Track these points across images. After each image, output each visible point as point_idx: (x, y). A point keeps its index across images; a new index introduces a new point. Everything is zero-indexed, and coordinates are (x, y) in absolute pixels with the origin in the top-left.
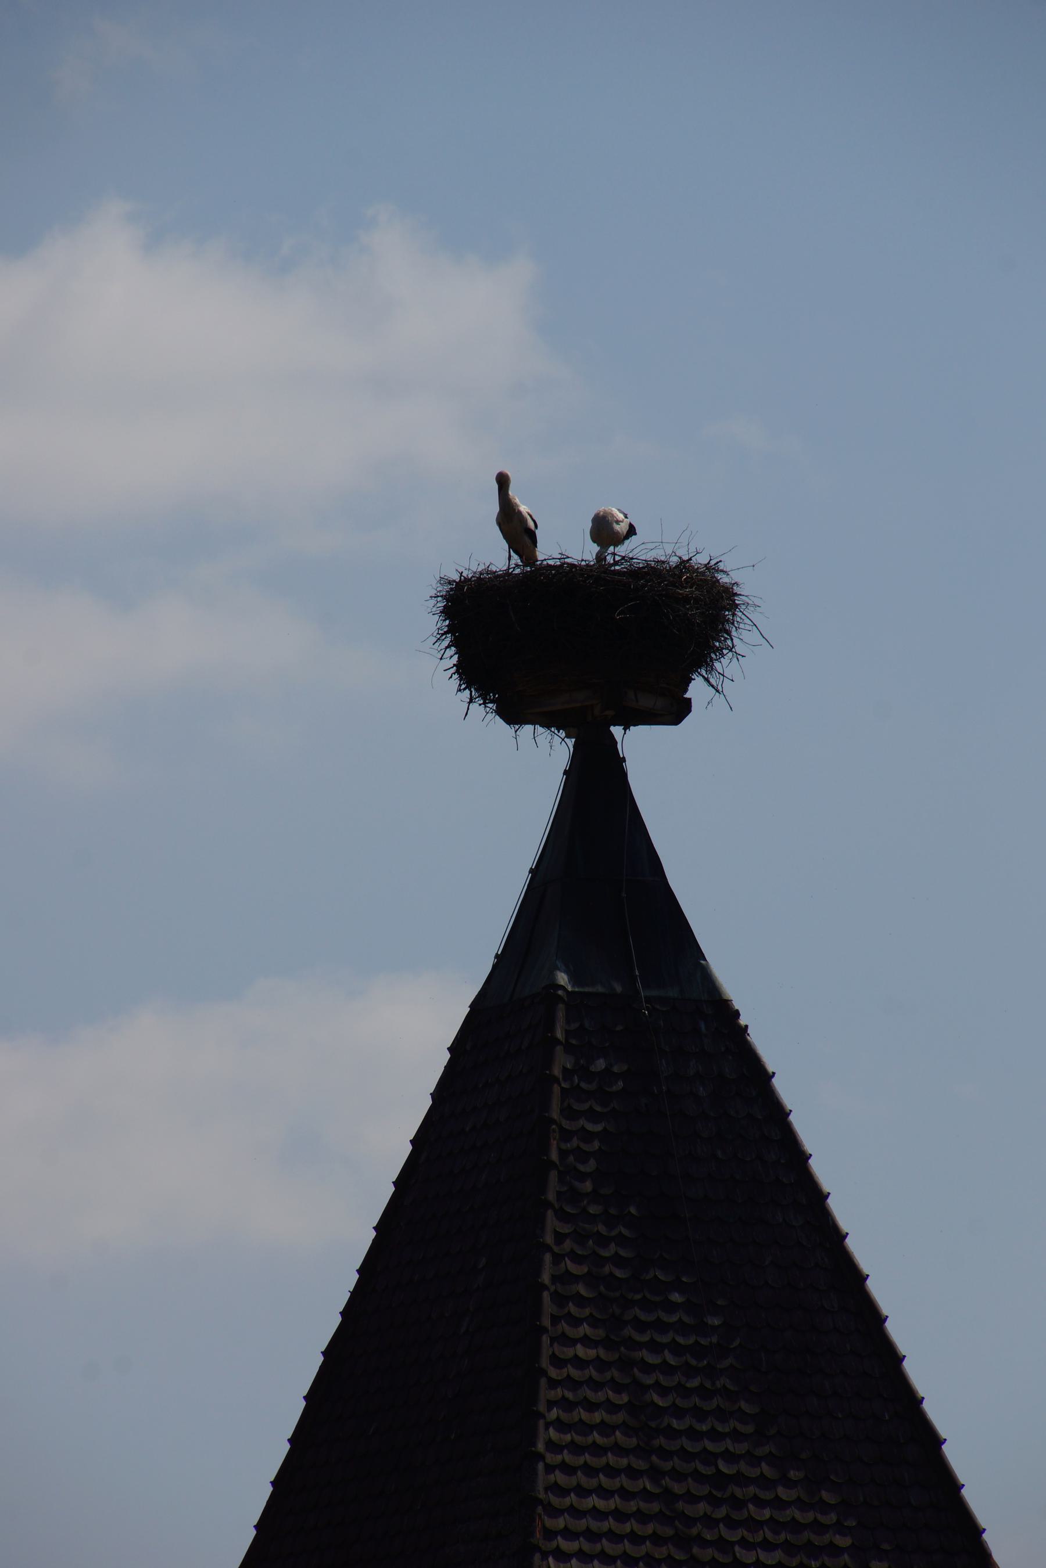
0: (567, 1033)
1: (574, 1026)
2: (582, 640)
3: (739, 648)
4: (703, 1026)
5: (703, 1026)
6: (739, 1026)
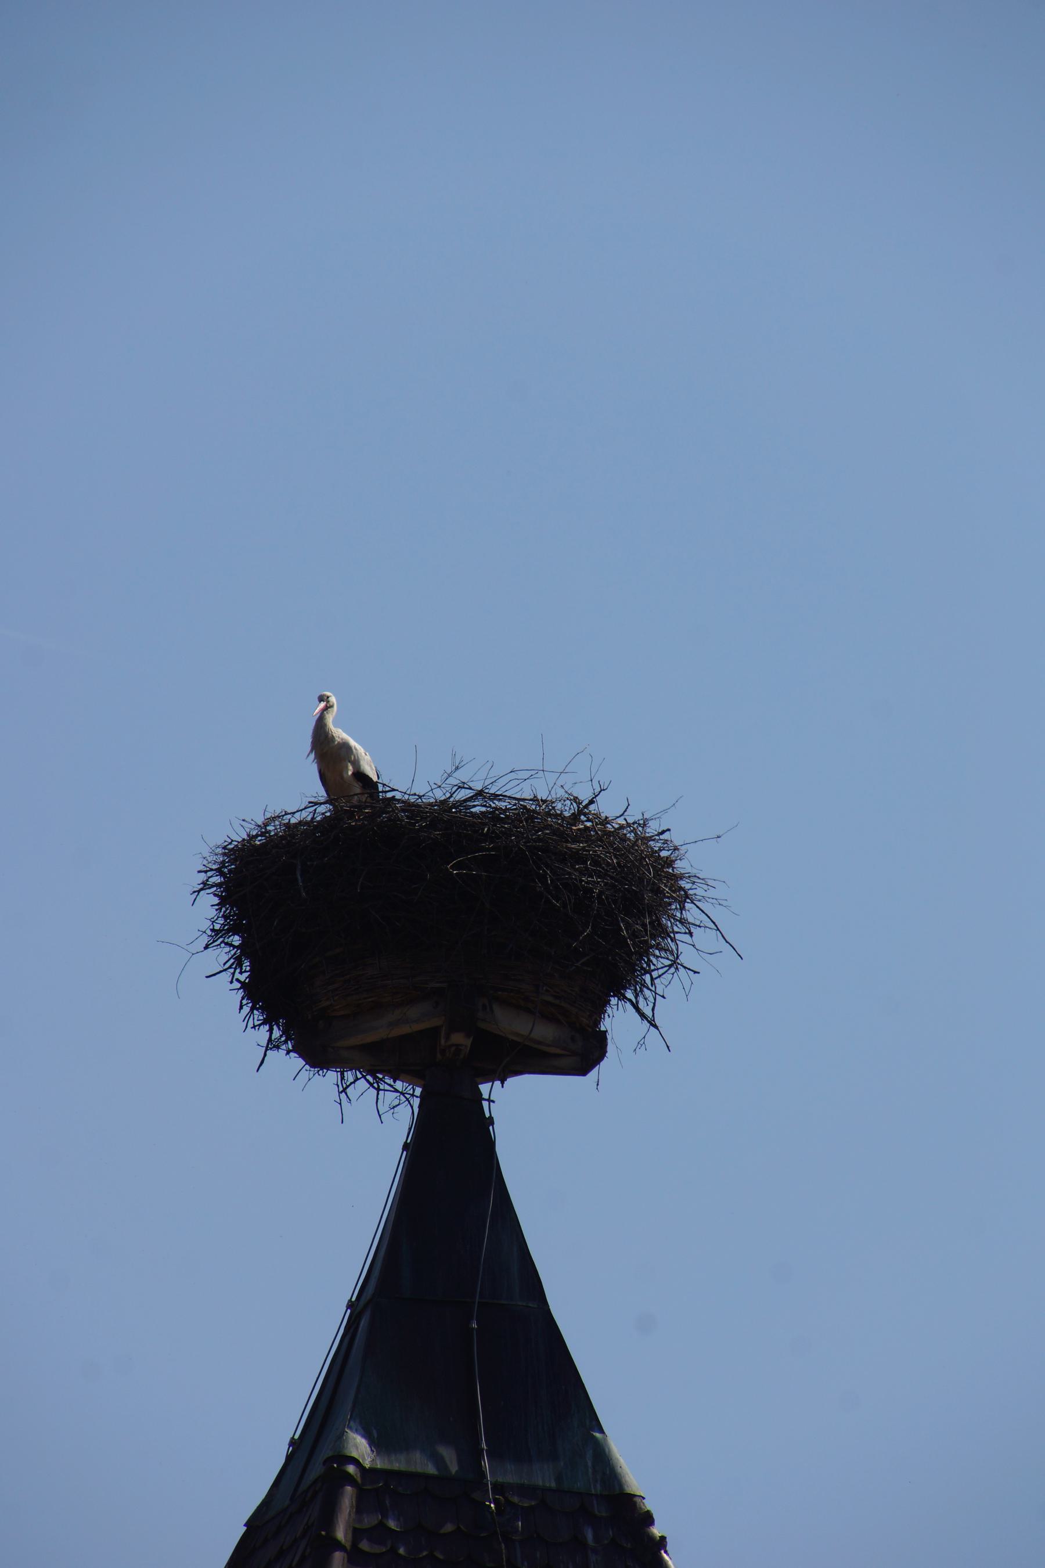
0: (357, 1534)
1: (370, 1521)
2: (438, 936)
3: (687, 956)
4: (589, 1535)
5: (589, 1535)
6: (651, 1538)
